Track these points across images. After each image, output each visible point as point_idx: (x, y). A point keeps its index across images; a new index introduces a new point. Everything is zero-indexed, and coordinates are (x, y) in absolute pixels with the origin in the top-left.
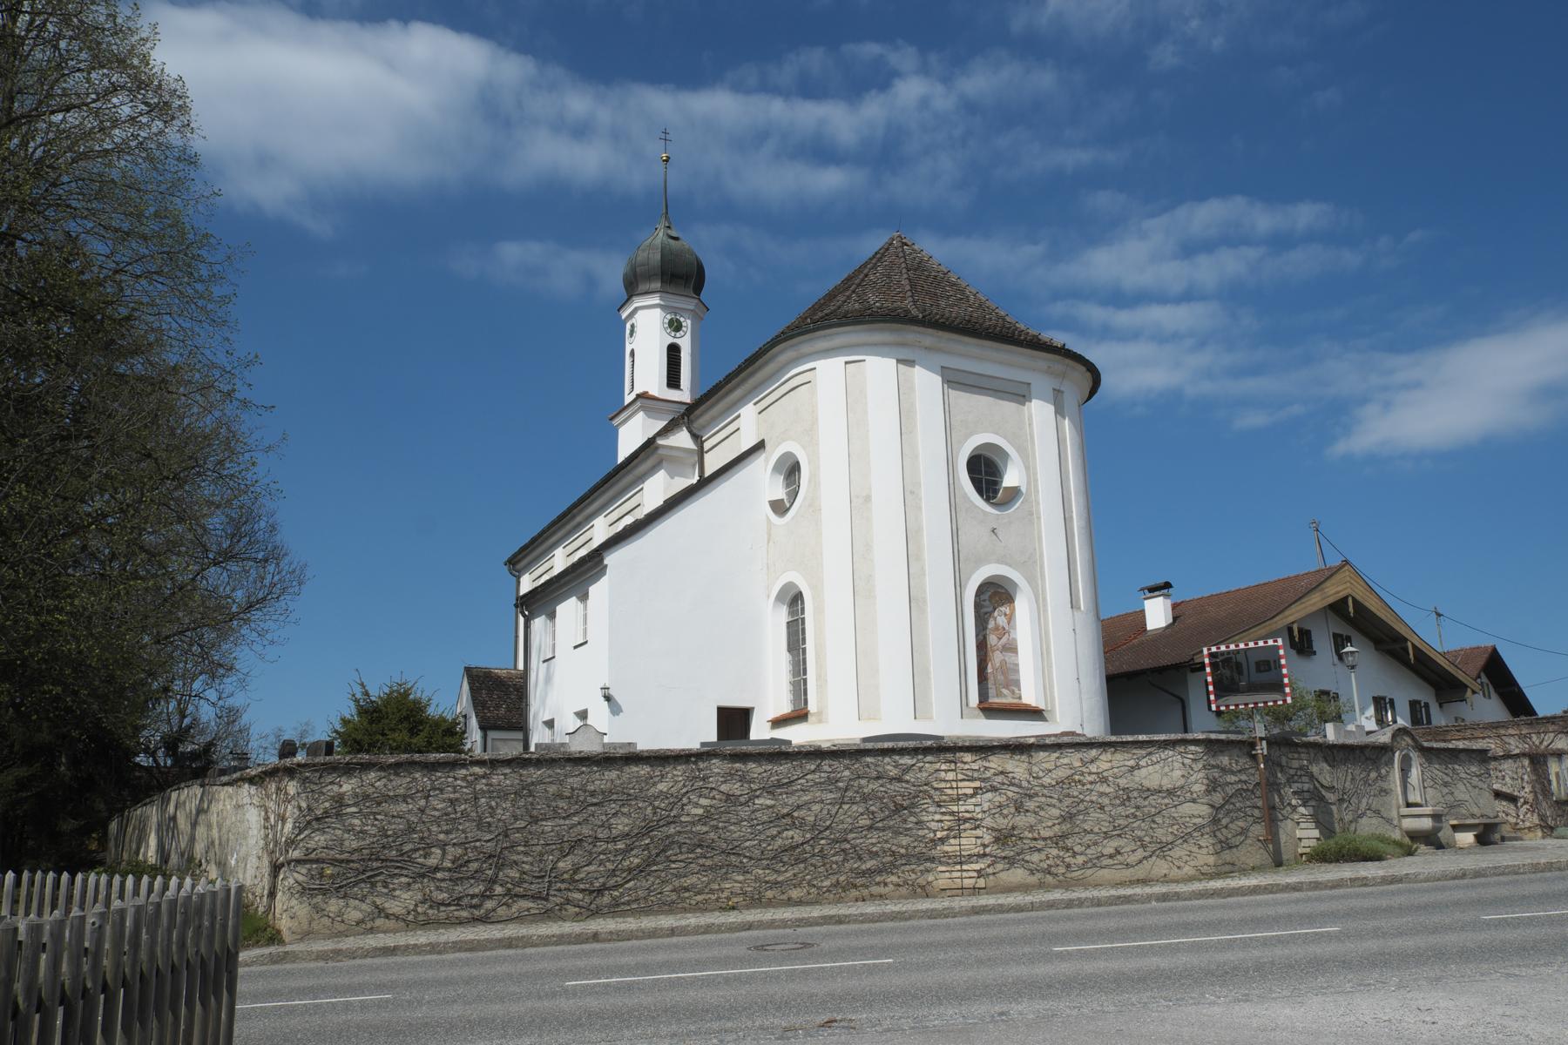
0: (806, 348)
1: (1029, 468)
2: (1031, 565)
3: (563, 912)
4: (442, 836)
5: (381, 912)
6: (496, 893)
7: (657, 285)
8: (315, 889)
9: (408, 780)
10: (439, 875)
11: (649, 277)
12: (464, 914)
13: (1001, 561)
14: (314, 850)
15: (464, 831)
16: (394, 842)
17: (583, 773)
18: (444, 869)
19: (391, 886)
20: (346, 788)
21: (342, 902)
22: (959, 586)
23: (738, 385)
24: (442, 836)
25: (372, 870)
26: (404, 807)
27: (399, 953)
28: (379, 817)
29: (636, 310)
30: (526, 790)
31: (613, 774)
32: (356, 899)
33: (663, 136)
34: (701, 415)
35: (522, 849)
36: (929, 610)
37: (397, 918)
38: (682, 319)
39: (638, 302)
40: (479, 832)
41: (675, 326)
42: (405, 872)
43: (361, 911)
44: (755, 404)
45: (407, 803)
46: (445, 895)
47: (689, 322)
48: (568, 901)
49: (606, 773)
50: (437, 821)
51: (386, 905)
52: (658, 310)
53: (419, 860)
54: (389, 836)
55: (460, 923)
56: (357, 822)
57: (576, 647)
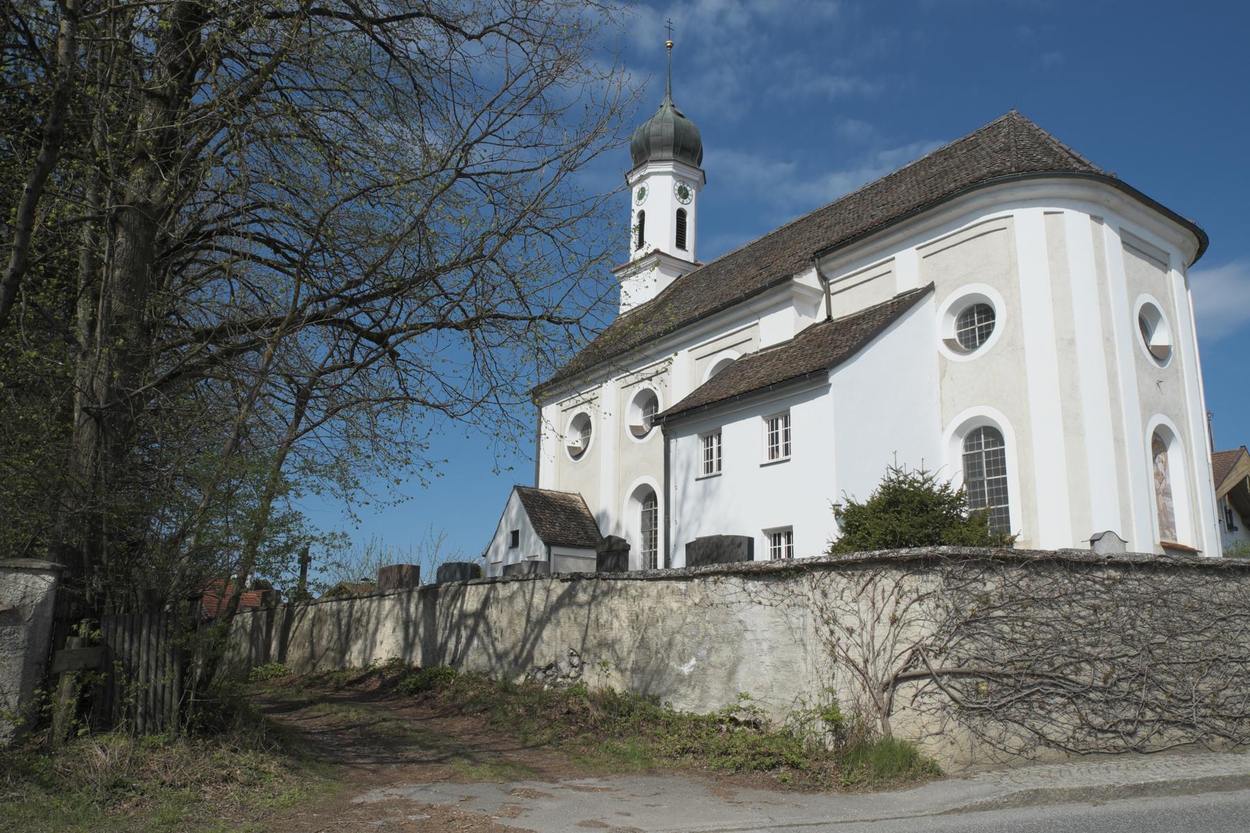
0: (1005, 196)
1: (1173, 330)
2: (1179, 417)
3: (1210, 742)
4: (1088, 649)
5: (1042, 738)
6: (1147, 718)
7: (670, 154)
8: (973, 709)
9: (1050, 581)
10: (1092, 695)
11: (662, 146)
12: (1120, 742)
13: (633, 443)
14: (968, 660)
15: (1110, 645)
16: (1044, 653)
17: (1207, 583)
18: (1096, 689)
19: (1048, 708)
20: (990, 586)
21: (1000, 726)
22: (1145, 432)
23: (899, 230)
24: (1088, 649)
25: (1029, 687)
26: (1048, 613)
27: (1149, 792)
28: (1027, 624)
29: (649, 175)
30: (1160, 598)
31: (1233, 586)
32: (1015, 722)
33: (668, 25)
34: (834, 258)
35: (1164, 667)
36: (1127, 450)
37: (1058, 745)
38: (688, 188)
39: (651, 168)
40: (1123, 646)
41: (683, 193)
42: (1061, 691)
43: (1021, 736)
44: (918, 249)
45: (1052, 609)
46: (1100, 719)
47: (694, 191)
48: (1215, 730)
49: (1228, 584)
50: (1084, 631)
51: (1046, 730)
52: (670, 177)
53: (1070, 677)
54: (1040, 647)
55: (1118, 754)
56: (1006, 629)
57: (762, 466)
